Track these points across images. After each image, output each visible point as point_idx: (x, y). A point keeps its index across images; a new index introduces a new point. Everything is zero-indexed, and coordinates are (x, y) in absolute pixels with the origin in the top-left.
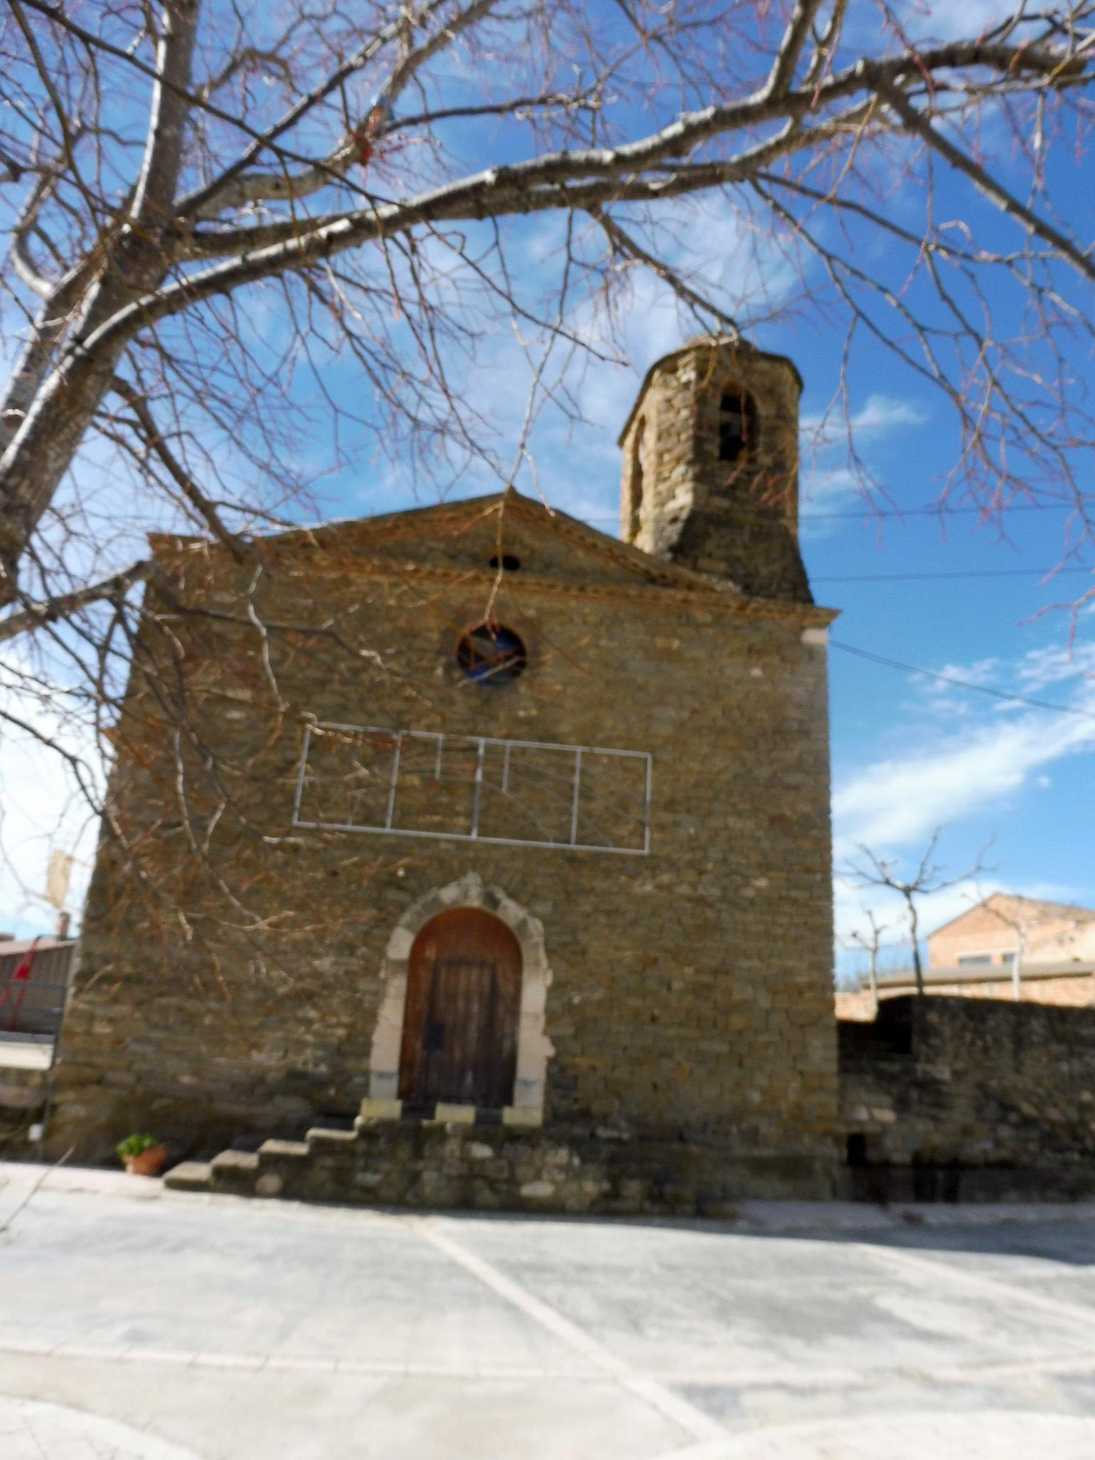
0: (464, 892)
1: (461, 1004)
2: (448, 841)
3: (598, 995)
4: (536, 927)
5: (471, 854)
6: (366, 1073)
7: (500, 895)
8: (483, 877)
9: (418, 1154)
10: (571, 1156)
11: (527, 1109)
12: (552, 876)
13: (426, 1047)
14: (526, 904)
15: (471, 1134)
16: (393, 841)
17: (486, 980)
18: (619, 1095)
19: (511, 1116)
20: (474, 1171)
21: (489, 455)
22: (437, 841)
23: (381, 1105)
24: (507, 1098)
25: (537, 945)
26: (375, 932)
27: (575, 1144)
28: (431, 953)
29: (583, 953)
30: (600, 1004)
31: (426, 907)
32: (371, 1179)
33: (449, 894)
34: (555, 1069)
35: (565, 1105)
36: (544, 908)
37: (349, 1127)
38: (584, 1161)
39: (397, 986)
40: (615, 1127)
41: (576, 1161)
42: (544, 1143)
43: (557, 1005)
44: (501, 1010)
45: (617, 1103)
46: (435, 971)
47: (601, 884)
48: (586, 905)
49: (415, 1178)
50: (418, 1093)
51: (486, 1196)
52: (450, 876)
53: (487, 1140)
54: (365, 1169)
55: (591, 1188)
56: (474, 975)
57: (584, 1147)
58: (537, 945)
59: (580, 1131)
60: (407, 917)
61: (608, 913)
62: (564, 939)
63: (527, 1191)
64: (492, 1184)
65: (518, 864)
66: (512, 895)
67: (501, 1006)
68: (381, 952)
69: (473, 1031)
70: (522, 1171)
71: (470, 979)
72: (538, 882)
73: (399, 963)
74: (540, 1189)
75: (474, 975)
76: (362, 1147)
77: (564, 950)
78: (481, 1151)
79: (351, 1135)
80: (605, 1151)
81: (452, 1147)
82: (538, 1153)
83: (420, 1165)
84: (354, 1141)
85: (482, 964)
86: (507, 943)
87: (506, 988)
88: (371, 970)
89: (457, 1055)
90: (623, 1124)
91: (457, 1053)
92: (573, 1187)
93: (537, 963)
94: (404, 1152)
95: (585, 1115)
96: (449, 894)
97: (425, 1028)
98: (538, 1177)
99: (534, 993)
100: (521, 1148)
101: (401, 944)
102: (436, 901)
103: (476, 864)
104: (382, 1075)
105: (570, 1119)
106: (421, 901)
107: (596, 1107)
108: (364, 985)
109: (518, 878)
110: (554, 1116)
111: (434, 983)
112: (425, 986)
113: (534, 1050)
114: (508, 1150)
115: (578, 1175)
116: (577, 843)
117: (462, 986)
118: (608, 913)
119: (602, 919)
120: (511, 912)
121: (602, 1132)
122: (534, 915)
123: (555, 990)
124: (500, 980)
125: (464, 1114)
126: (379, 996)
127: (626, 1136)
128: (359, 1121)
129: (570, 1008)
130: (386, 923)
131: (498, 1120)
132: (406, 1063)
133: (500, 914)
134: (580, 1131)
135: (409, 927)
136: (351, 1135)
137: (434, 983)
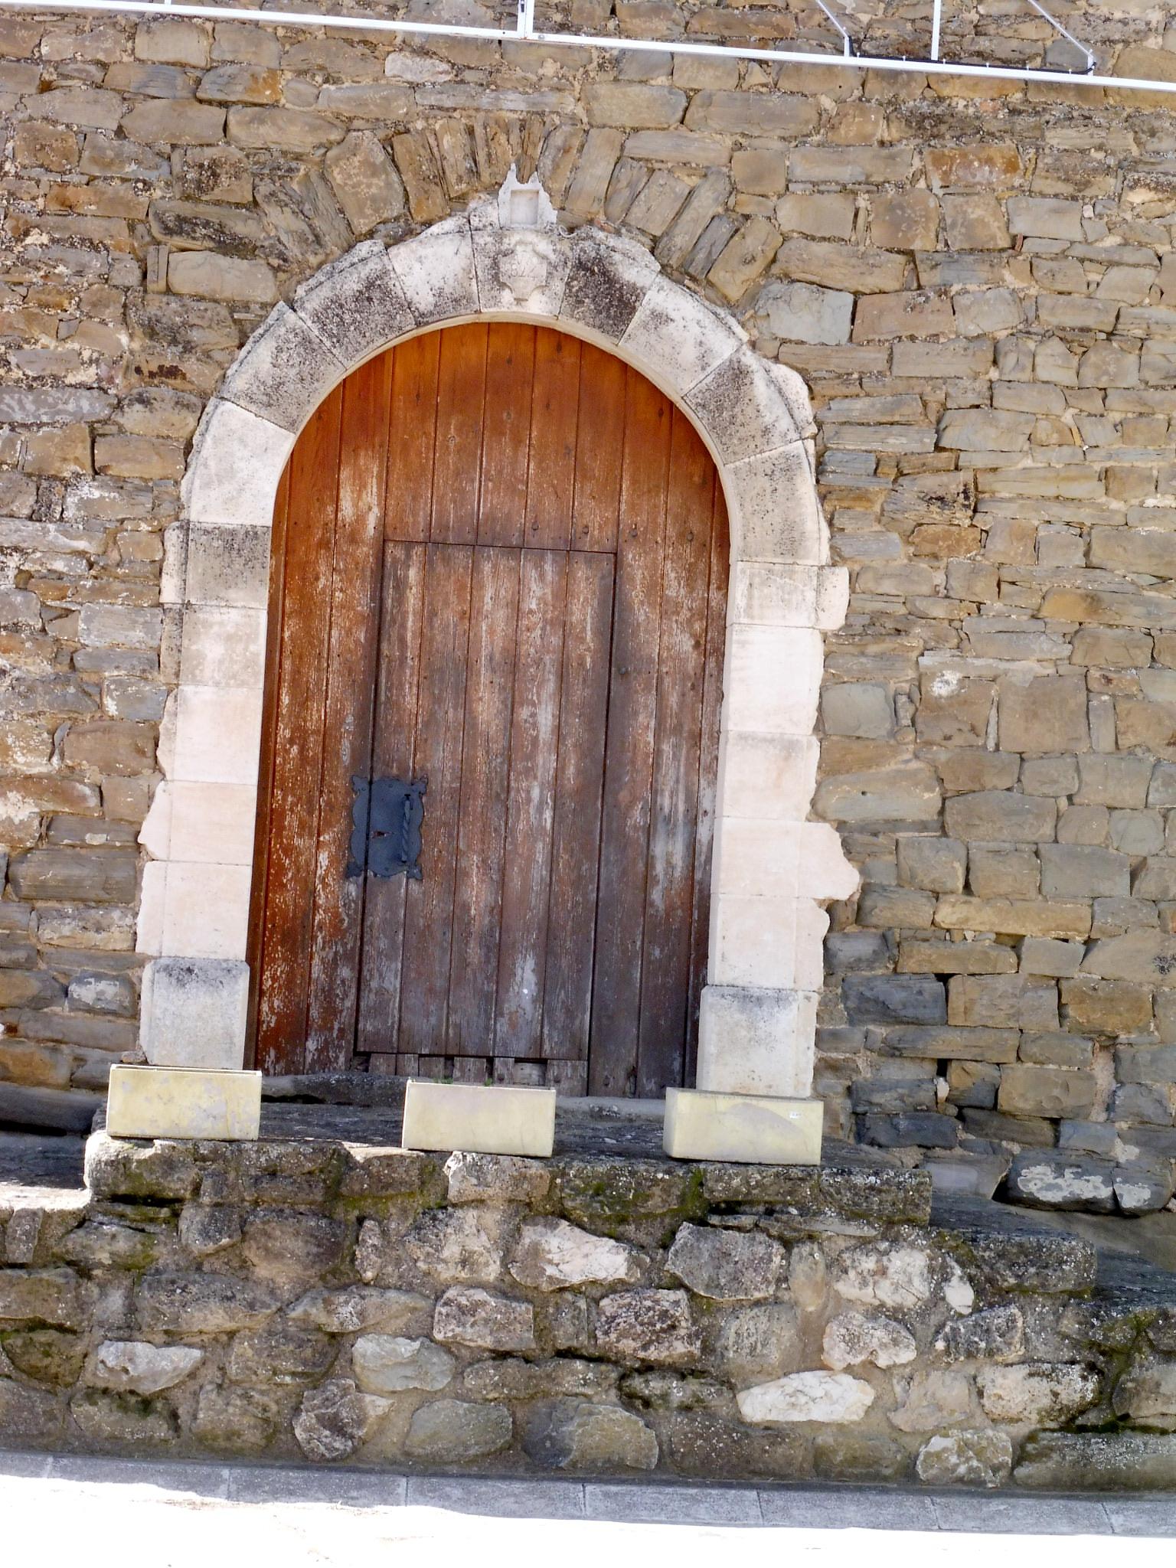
0: (485, 261)
1: (487, 707)
2: (423, 49)
3: (1033, 662)
4: (780, 396)
5: (513, 104)
6: (124, 966)
7: (636, 268)
8: (563, 199)
9: (335, 1268)
10: (940, 1275)
11: (755, 1094)
12: (846, 190)
13: (354, 867)
14: (741, 307)
15: (544, 1199)
16: (193, 50)
17: (584, 612)
18: (1109, 1044)
19: (696, 1123)
20: (555, 1339)
21: (525, 133)
22: (369, 44)
23: (186, 1084)
24: (674, 1054)
25: (788, 468)
26: (134, 417)
27: (950, 1227)
28: (360, 501)
29: (974, 499)
30: (1039, 697)
31: (336, 318)
32: (154, 1363)
33: (428, 269)
34: (858, 946)
35: (900, 1080)
36: (814, 320)
37: (68, 1175)
38: (990, 1294)
39: (232, 632)
40: (1096, 1161)
41: (960, 1295)
42: (830, 1224)
43: (866, 702)
44: (643, 727)
45: (1102, 1072)
46: (381, 574)
47: (1044, 223)
48: (987, 307)
49: (331, 1350)
50: (323, 1047)
51: (604, 1423)
52: (432, 192)
53: (610, 1218)
54: (128, 1330)
55: (1018, 1393)
56: (538, 590)
57: (991, 1238)
58: (788, 468)
59: (959, 1176)
60: (260, 359)
61: (1077, 340)
62: (896, 443)
63: (761, 1404)
64: (630, 1382)
65: (709, 145)
66: (682, 273)
67: (642, 709)
68: (165, 506)
69: (535, 805)
70: (741, 1332)
71: (520, 606)
72: (789, 215)
73: (231, 541)
74: (826, 1400)
75: (538, 590)
76: (112, 1242)
77: (904, 483)
78: (584, 1257)
79: (75, 1200)
80: (1079, 1249)
81: (470, 1239)
82: (807, 1261)
83: (345, 1311)
84: (81, 1220)
85: (568, 550)
86: (672, 448)
87: (668, 641)
88: (135, 580)
89: (477, 893)
90: (1125, 1153)
91: (470, 902)
92: (949, 1388)
93: (790, 544)
94: (281, 1262)
95: (978, 1113)
96: (428, 269)
97: (350, 800)
98: (809, 1357)
99: (777, 657)
100: (740, 1245)
101: (240, 468)
102: (375, 290)
103: (532, 144)
104: (183, 972)
105: (931, 1135)
106: (315, 297)
107: (1020, 1092)
108: (100, 628)
109: (707, 203)
110: (859, 1126)
111: (379, 622)
112: (344, 636)
113: (774, 882)
114: (692, 1253)
115: (967, 1347)
116: (951, 57)
117: (492, 632)
118: (1077, 340)
119: (1053, 363)
120: (680, 340)
121: (1039, 1181)
122: (780, 351)
123: (865, 636)
124: (642, 612)
125: (521, 1118)
126: (160, 669)
127: (1133, 1197)
128: (98, 1147)
129: (916, 710)
130: (174, 370)
131: (645, 1144)
132: (273, 930)
133: (633, 347)
134: (959, 1176)
135: (269, 399)
136: (75, 1200)
137: (379, 622)
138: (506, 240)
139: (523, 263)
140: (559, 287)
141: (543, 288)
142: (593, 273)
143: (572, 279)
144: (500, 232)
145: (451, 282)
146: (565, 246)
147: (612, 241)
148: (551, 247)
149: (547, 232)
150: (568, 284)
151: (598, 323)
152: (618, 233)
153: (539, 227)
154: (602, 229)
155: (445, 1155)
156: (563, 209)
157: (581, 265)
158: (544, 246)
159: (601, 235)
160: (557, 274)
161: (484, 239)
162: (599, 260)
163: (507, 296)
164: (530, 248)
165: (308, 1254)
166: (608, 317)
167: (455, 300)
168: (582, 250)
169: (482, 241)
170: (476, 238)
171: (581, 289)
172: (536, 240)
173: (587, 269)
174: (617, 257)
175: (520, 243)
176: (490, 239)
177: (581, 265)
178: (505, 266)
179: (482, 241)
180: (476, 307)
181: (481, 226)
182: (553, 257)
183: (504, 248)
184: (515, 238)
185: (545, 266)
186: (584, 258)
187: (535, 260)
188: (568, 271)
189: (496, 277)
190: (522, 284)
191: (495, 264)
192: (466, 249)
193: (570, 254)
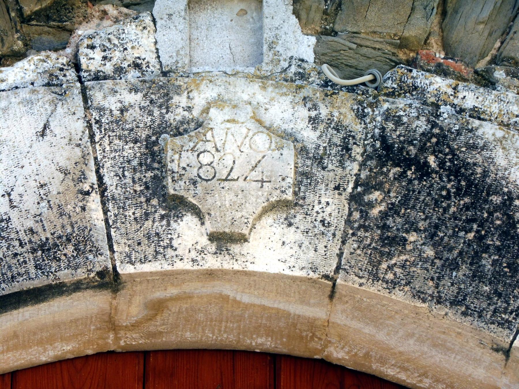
138: (180, 100)
139: (231, 147)
140: (331, 205)
141: (284, 208)
142: (424, 171)
143: (369, 186)
144: (162, 84)
145: (30, 202)
146: (344, 109)
147: (470, 97)
148: (304, 113)
149: (295, 79)
150: (354, 198)
151: (448, 290)
152: (485, 81)
153: (266, 68)
154: (442, 71)
155: (310, 117)
156: (326, 33)
157: (387, 152)
158: (284, 111)
159: (440, 84)
160: (332, 172)
161: (118, 98)
162: (439, 139)
163: (189, 232)
164: (244, 114)
165: (478, 321)
166: (477, 275)
167: (43, 246)
168: (388, 116)
169: (112, 104)
170: (98, 97)
171: (393, 210)
172: (261, 97)
173: (407, 162)
174: (488, 131)
175: (219, 102)
176: (134, 99)
177: (387, 152)
178: (179, 157)
179: (112, 104)
180: (102, 262)
181: (109, 68)
182: (310, 136)
183: (175, 116)
184: (201, 97)
185: (289, 153)
186: (395, 135)
187: (262, 141)
188: (354, 167)
189: (156, 188)
190: (229, 198)
191: (153, 155)
192: (69, 121)
193: (358, 128)
